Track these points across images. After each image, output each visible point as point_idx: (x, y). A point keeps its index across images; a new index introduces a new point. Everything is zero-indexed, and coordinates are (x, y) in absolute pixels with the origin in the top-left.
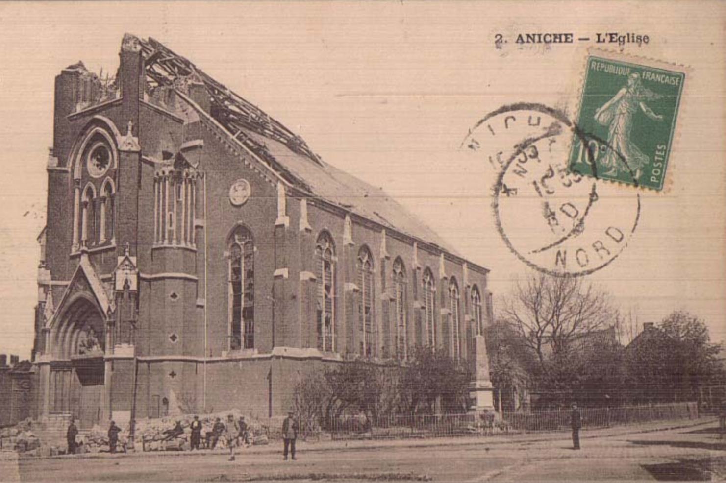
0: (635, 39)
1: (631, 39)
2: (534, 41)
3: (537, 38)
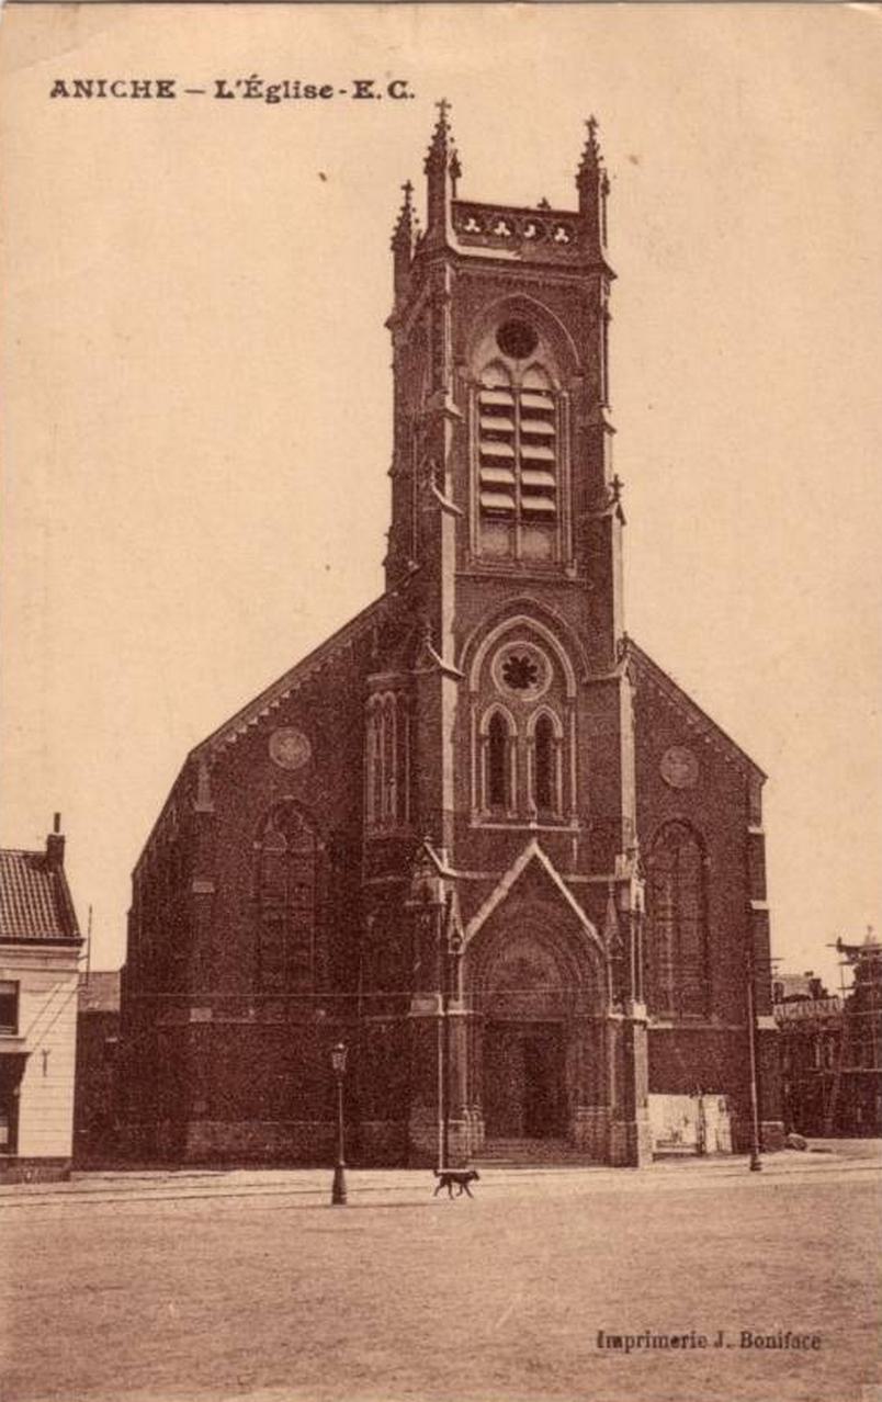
0: (302, 92)
1: (292, 92)
2: (89, 94)
3: (95, 88)
